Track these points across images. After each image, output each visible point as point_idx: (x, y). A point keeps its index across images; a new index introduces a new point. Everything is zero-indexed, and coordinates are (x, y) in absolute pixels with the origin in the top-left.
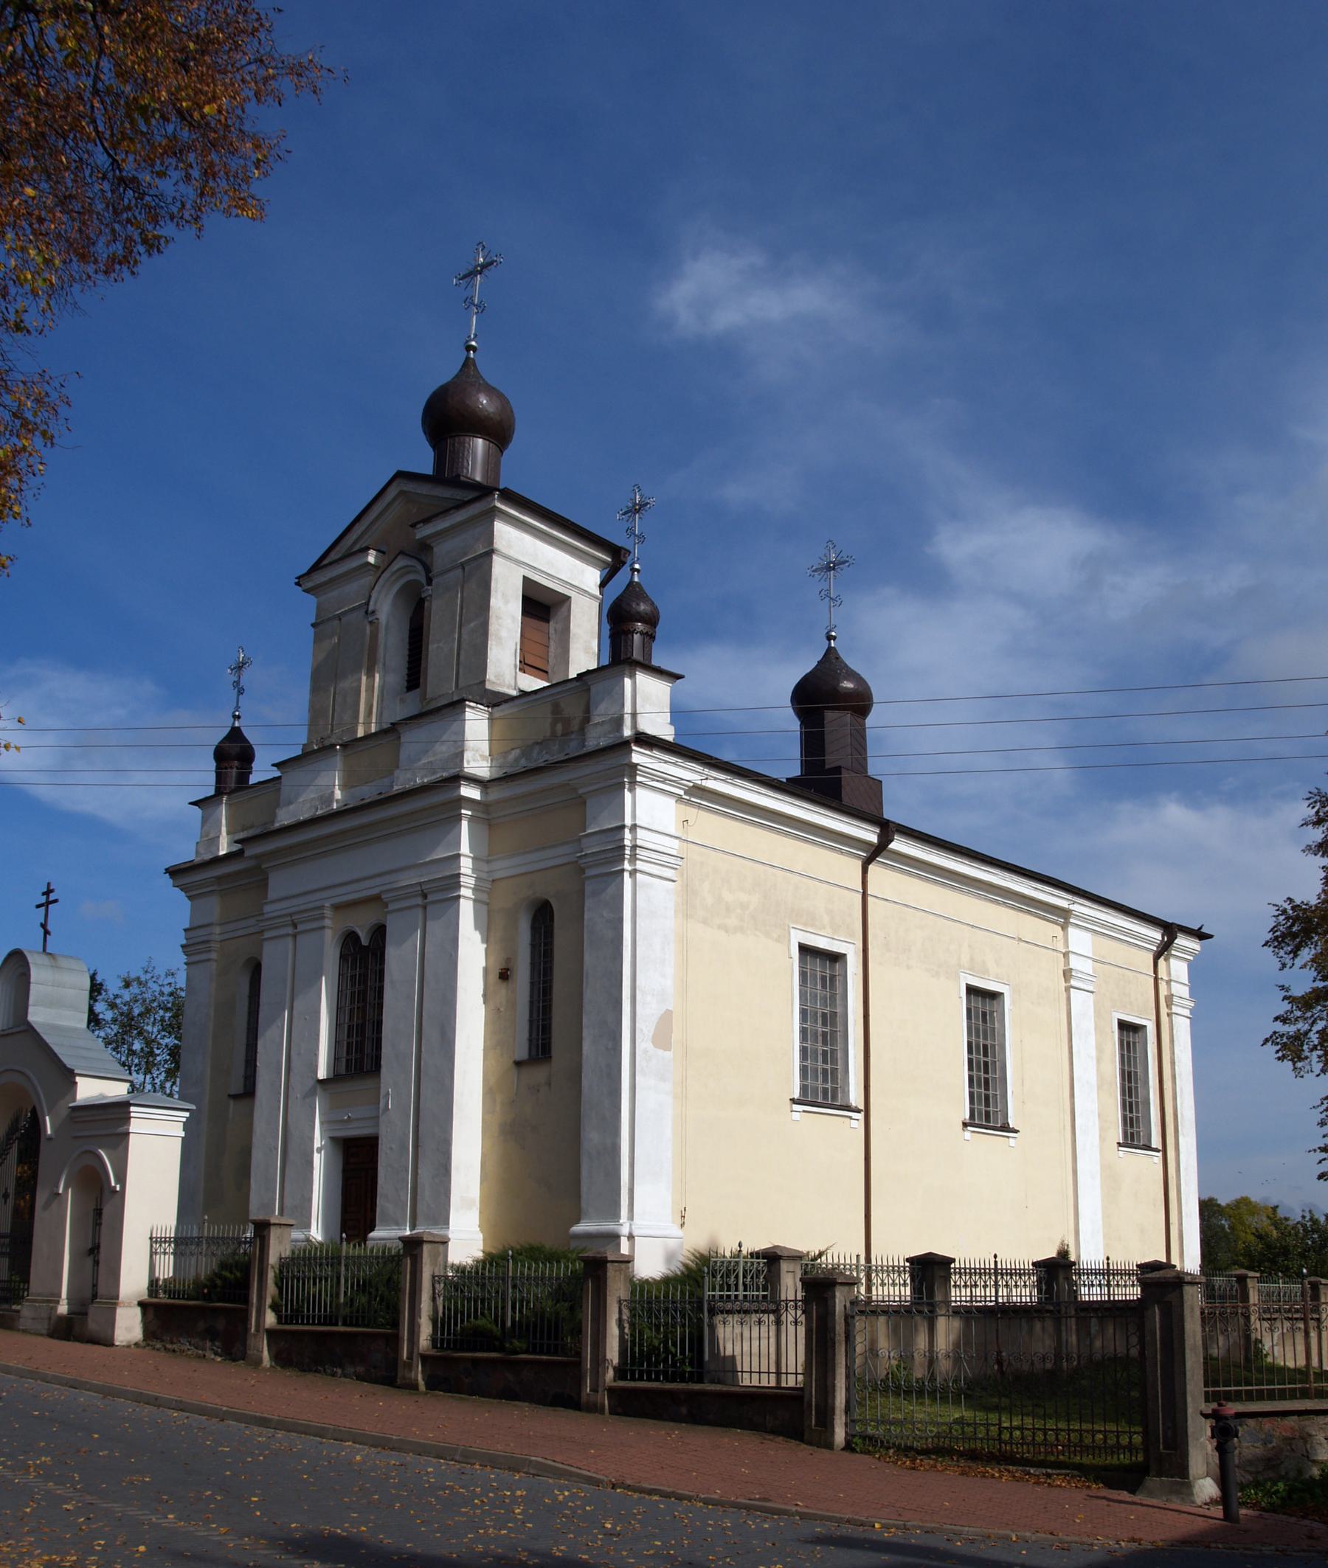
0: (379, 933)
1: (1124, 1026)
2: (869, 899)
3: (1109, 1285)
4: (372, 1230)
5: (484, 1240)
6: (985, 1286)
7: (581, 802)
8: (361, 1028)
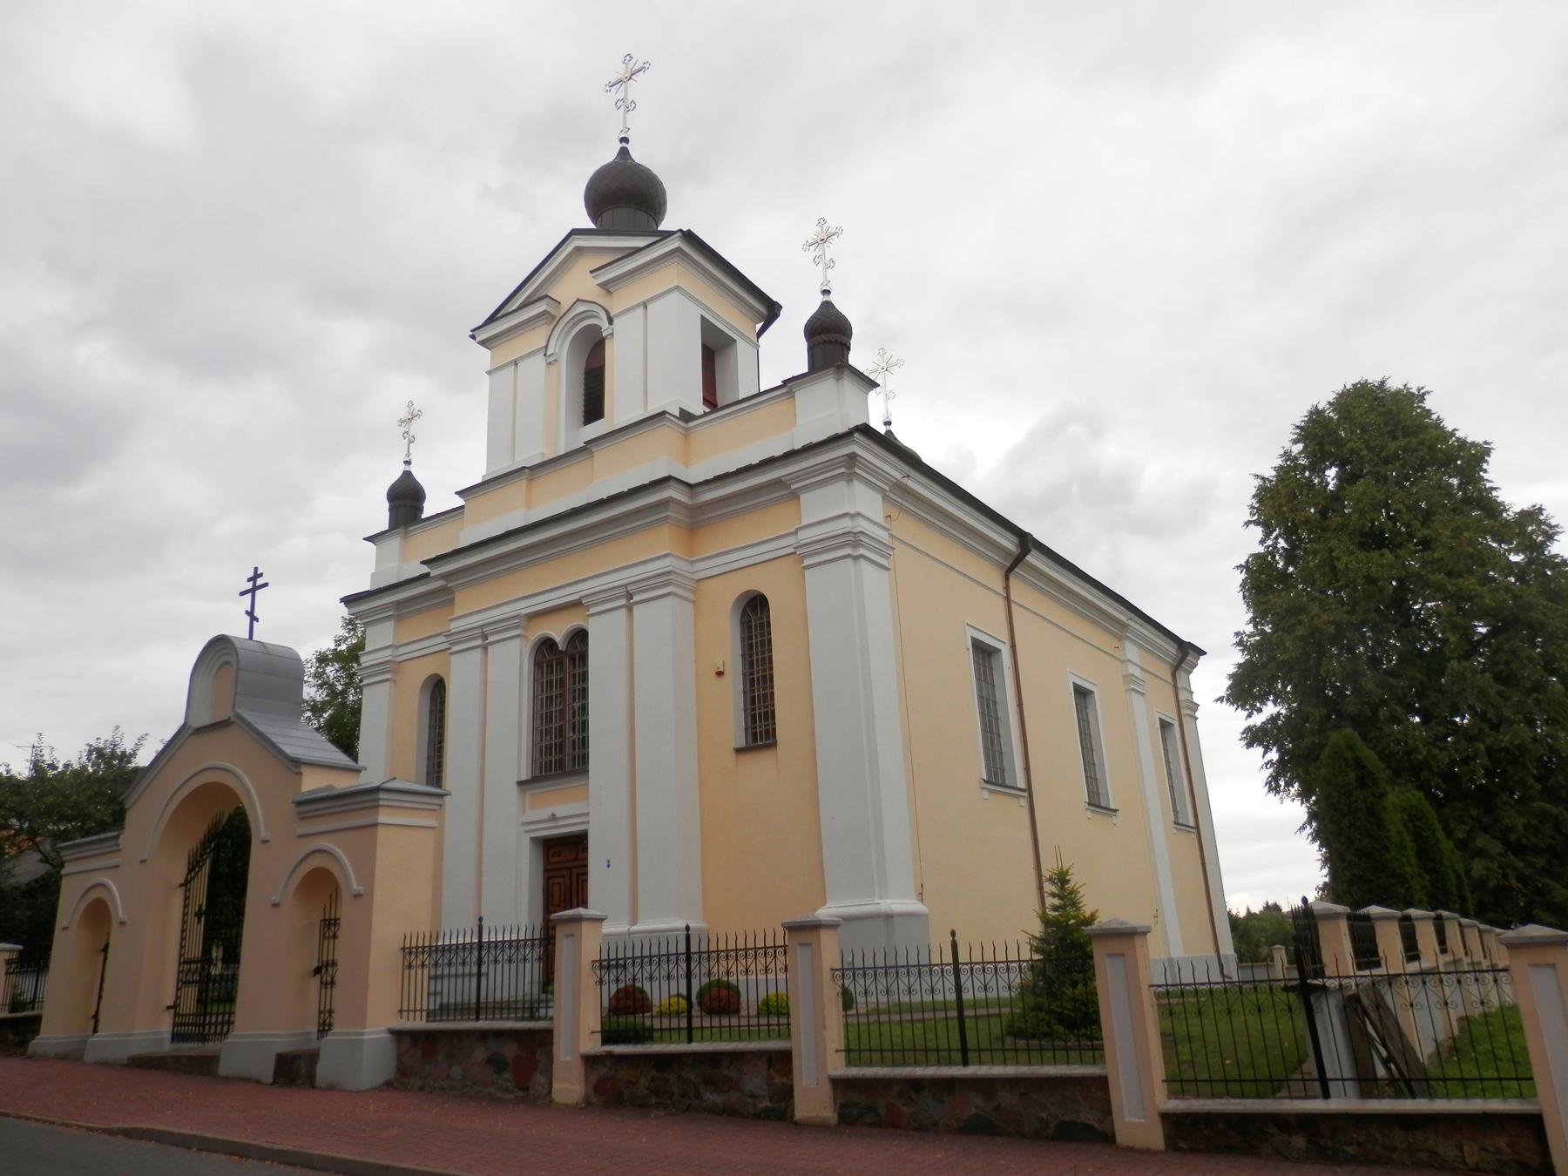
2: (1013, 606)
5: (1326, 861)
7: (795, 496)
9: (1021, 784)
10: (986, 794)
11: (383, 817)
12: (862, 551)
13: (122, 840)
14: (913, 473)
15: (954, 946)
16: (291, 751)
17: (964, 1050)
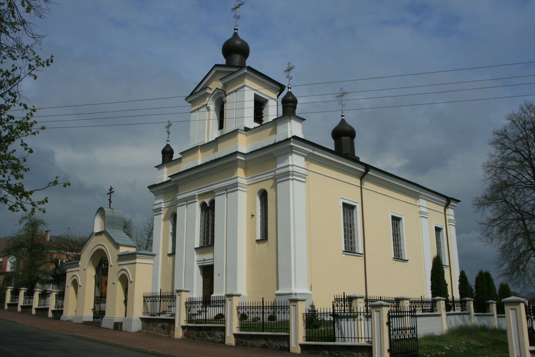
0: (213, 202)
2: (363, 189)
4: (212, 293)
7: (275, 159)
9: (361, 251)
10: (344, 255)
11: (138, 260)
12: (294, 177)
13: (80, 263)
14: (316, 149)
15: (263, 301)
16: (117, 241)
17: (263, 328)
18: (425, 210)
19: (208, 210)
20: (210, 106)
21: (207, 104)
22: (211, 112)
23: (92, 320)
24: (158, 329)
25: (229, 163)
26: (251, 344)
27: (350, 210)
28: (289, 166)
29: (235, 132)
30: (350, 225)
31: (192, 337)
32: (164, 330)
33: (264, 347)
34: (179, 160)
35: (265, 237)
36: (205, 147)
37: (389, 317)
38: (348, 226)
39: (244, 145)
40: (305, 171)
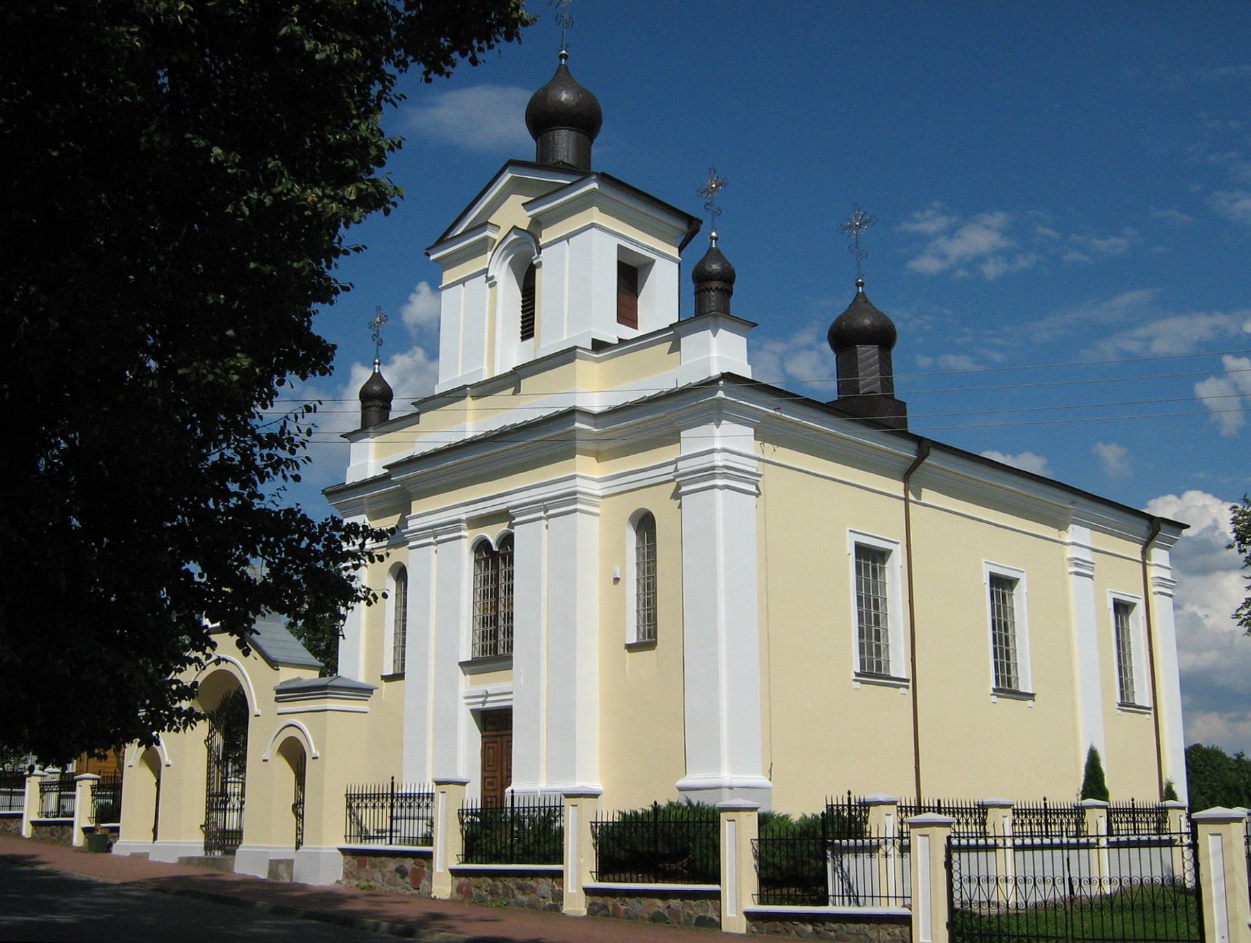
1: (863, 552)
3: (1134, 822)
6: (1022, 824)
8: (495, 621)
9: (905, 673)
14: (785, 404)
18: (1086, 555)
19: (495, 560)
20: (496, 274)
21: (486, 271)
22: (500, 286)
23: (201, 853)
24: (388, 876)
25: (552, 437)
26: (626, 912)
27: (874, 562)
28: (712, 451)
29: (567, 356)
30: (876, 601)
31: (480, 896)
32: (402, 877)
33: (657, 918)
34: (411, 419)
35: (647, 641)
36: (486, 389)
37: (950, 849)
38: (868, 605)
39: (594, 389)
40: (756, 463)
